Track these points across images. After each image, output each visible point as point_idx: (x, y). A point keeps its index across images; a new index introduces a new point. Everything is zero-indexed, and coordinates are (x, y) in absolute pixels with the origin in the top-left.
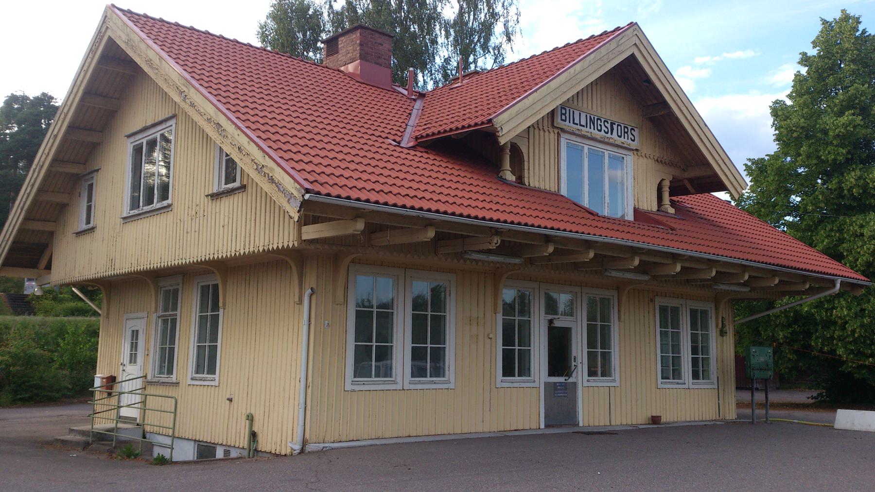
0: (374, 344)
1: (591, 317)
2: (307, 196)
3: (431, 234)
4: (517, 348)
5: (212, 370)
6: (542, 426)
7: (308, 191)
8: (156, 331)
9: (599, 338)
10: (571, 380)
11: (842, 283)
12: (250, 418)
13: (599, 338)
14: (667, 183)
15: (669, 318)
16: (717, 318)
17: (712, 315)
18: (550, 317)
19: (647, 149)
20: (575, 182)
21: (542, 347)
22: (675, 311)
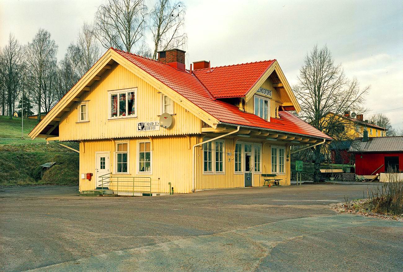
0: (238, 162)
1: (256, 153)
2: (220, 123)
3: (250, 131)
4: (122, 163)
5: (125, 170)
6: (244, 186)
7: (220, 121)
8: (115, 158)
9: (257, 159)
10: (251, 172)
11: (240, 128)
12: (170, 184)
13: (257, 159)
14: (278, 108)
15: (274, 153)
16: (286, 152)
17: (285, 150)
18: (246, 152)
19: (274, 98)
20: (257, 111)
21: (98, 164)
22: (276, 149)
